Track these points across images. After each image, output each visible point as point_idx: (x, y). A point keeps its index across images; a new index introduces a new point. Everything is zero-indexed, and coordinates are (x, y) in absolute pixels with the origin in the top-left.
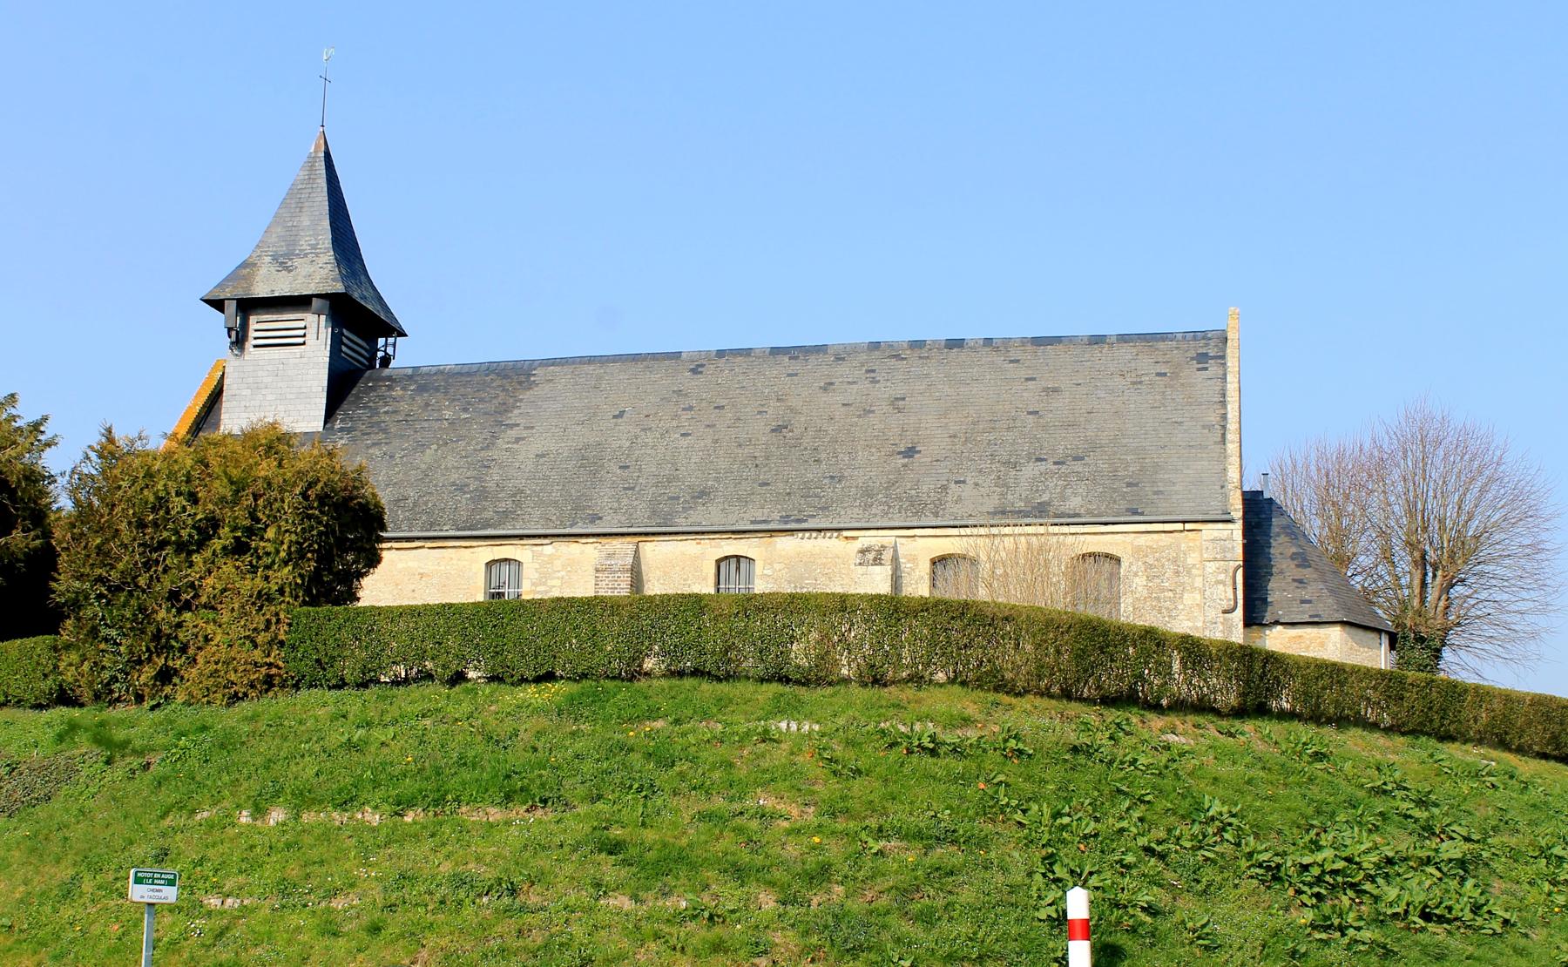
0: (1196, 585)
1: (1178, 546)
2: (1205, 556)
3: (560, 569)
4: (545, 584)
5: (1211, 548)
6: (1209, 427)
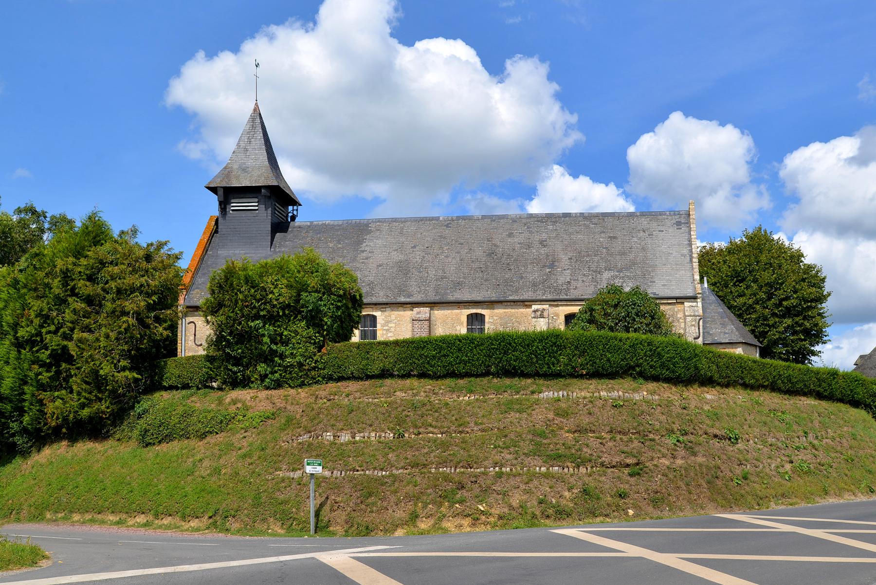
1: (674, 310)
2: (686, 314)
4: (387, 326)
6: (684, 256)
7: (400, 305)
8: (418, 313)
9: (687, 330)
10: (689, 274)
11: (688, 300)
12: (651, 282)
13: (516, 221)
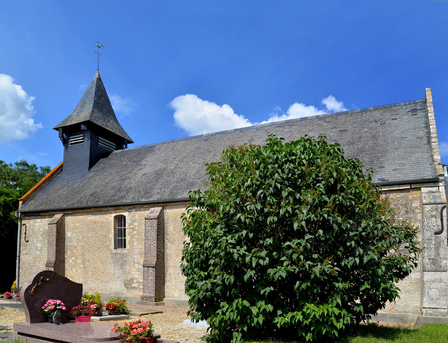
0: (418, 218)
1: (407, 198)
2: (424, 201)
3: (137, 218)
4: (133, 225)
5: (427, 196)
6: (421, 138)
7: (141, 206)
8: (152, 212)
9: (425, 223)
10: (427, 155)
11: (426, 185)
12: (379, 167)
13: (259, 130)
